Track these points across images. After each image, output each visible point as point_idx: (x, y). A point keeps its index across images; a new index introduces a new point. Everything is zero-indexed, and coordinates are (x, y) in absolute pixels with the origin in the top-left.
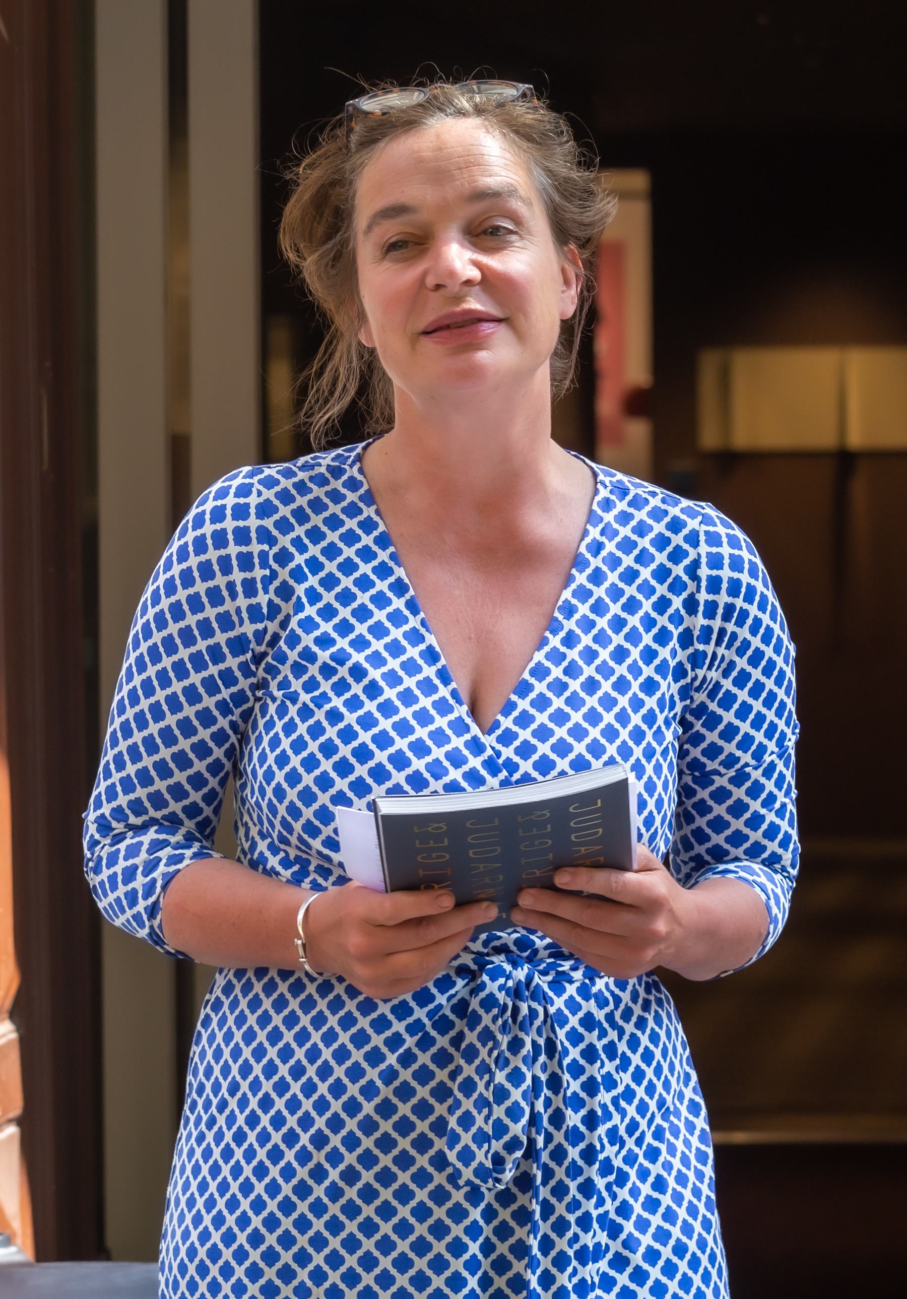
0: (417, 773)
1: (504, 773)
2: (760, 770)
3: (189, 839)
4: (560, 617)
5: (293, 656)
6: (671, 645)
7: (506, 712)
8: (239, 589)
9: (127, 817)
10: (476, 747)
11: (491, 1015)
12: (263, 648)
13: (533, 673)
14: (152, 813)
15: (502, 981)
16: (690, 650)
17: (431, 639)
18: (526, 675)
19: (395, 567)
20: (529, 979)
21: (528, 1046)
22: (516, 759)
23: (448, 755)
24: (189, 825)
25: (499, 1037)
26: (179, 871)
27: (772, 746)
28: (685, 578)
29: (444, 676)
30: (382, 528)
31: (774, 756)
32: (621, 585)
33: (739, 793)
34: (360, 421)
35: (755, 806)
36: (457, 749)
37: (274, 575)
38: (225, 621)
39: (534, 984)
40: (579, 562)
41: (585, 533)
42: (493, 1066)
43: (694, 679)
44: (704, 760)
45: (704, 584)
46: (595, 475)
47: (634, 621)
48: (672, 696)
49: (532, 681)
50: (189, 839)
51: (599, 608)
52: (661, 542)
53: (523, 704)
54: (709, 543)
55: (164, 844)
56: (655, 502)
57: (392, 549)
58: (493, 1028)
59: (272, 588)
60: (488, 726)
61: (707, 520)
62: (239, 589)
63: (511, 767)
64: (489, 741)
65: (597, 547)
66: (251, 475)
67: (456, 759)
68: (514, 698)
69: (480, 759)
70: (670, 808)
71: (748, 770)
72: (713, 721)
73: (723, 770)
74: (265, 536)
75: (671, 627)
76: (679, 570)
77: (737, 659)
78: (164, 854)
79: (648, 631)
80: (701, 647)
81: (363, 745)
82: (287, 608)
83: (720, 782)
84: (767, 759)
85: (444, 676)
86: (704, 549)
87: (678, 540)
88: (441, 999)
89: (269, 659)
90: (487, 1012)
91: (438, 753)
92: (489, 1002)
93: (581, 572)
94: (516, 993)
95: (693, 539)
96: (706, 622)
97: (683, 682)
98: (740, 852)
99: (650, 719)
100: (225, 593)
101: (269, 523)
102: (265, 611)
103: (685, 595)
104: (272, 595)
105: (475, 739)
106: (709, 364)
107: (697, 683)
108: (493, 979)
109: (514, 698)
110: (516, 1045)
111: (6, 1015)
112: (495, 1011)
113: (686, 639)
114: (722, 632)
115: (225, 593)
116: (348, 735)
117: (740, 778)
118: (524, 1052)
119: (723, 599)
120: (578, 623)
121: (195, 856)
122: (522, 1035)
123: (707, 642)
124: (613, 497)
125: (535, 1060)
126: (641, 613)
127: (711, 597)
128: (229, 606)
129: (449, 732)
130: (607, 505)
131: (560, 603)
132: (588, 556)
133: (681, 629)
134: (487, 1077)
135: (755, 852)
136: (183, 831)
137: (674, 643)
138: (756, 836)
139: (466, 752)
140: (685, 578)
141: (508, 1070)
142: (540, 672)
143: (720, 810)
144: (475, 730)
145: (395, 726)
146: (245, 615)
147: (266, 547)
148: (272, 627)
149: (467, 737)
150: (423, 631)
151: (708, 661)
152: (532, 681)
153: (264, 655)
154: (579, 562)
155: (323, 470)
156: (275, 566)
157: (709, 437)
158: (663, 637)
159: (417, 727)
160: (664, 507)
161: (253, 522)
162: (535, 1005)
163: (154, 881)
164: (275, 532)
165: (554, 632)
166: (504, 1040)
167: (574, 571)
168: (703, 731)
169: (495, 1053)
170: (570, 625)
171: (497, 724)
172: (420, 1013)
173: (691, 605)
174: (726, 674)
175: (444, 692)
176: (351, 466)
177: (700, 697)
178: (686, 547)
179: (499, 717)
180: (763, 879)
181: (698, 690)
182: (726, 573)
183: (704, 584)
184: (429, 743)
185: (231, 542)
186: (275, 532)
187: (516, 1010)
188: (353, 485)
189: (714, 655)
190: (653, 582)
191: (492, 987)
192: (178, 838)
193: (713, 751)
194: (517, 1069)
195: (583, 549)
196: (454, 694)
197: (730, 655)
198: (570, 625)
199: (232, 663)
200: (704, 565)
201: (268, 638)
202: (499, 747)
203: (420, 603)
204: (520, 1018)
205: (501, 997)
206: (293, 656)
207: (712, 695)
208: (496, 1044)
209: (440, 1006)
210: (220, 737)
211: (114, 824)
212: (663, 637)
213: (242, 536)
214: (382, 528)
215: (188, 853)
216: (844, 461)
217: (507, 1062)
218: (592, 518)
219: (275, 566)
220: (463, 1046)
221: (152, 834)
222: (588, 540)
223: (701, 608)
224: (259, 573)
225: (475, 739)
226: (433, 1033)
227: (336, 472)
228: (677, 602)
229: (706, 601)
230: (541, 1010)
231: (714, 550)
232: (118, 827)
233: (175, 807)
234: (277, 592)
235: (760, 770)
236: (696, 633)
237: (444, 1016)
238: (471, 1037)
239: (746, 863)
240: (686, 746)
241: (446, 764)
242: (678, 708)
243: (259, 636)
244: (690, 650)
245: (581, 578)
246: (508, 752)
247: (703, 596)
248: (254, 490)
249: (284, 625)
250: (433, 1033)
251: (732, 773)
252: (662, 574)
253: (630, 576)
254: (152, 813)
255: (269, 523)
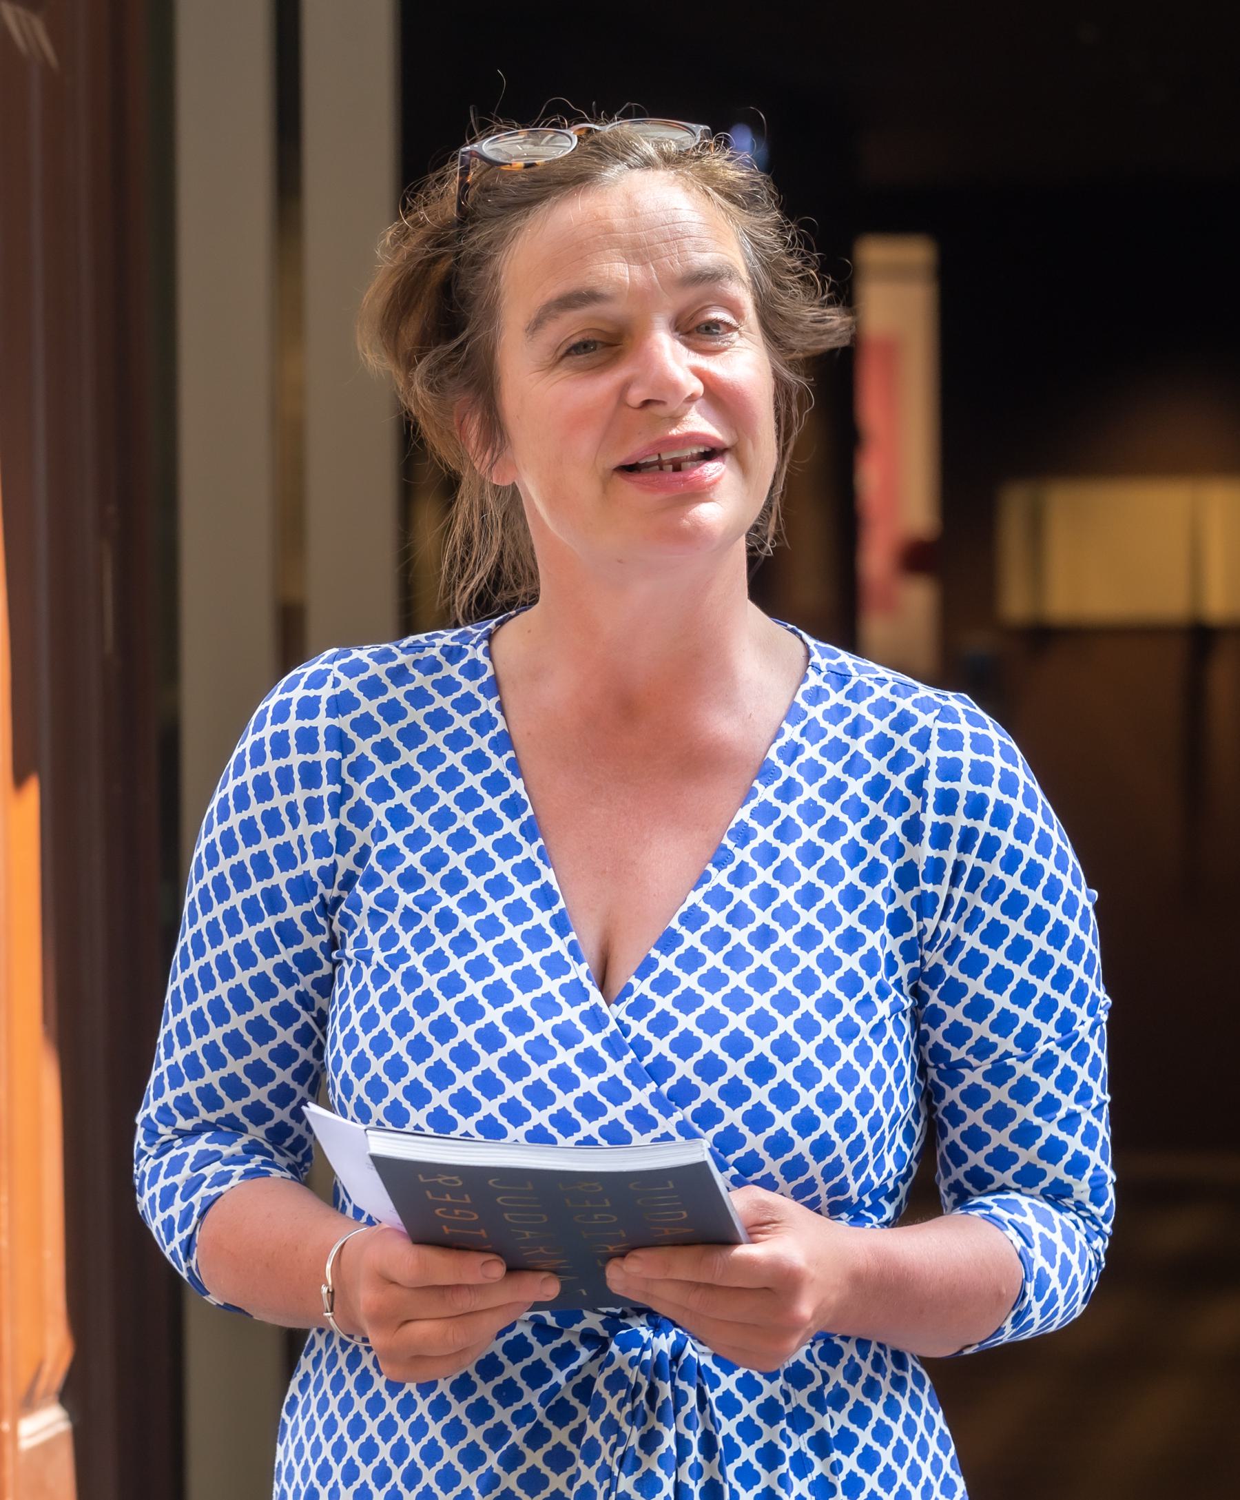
0: (513, 1055)
1: (631, 1055)
2: (1030, 1064)
3: (252, 1149)
4: (730, 845)
5: (368, 900)
6: (884, 883)
7: (642, 974)
8: (302, 812)
9: (175, 1119)
10: (595, 1020)
11: (617, 1398)
12: (335, 892)
13: (684, 920)
14: (204, 1115)
15: (636, 1352)
16: (915, 892)
17: (548, 875)
18: (675, 924)
19: (512, 779)
20: (678, 1350)
21: (669, 1440)
22: (649, 1036)
23: (556, 1031)
24: (257, 1133)
25: (626, 1429)
26: (221, 1194)
27: (1048, 1029)
28: (907, 793)
29: (561, 924)
30: (502, 725)
31: (1052, 1045)
32: (822, 802)
33: (999, 1094)
34: (505, 593)
35: (1026, 1113)
36: (569, 1023)
37: (347, 791)
38: (286, 857)
39: (684, 1356)
40: (767, 773)
41: (779, 733)
42: (616, 1470)
43: (922, 932)
44: (947, 1046)
45: (931, 800)
46: (809, 655)
47: (833, 850)
48: (890, 956)
49: (682, 931)
50: (252, 1149)
51: (786, 832)
52: (881, 745)
53: (667, 963)
54: (943, 745)
55: (216, 1156)
56: (881, 692)
57: (510, 754)
58: (620, 1417)
59: (344, 810)
60: (616, 992)
61: (947, 714)
62: (302, 812)
63: (641, 1047)
64: (616, 1012)
65: (791, 752)
66: (332, 660)
67: (567, 1036)
68: (655, 953)
69: (600, 1036)
70: (334, 1026)
71: (1009, 1061)
72: (954, 992)
73: (974, 1062)
74: (339, 741)
75: (884, 860)
76: (898, 782)
77: (985, 906)
78: (209, 1171)
79: (853, 865)
80: (929, 888)
81: (491, 1026)
82: (362, 837)
83: (973, 1077)
84: (1041, 1047)
85: (561, 924)
86: (935, 752)
87: (903, 741)
88: (559, 1377)
89: (343, 907)
90: (613, 1394)
91: (543, 1027)
92: (617, 1381)
93: (767, 785)
94: (657, 1369)
95: (922, 741)
96: (935, 853)
97: (907, 936)
98: (1006, 1177)
99: (851, 984)
100: (285, 818)
101: (344, 722)
102: (333, 840)
103: (906, 816)
104: (344, 819)
105: (595, 1009)
106: (1014, 504)
107: (927, 938)
108: (624, 1350)
109: (655, 953)
110: (650, 1441)
111: (53, 1397)
112: (622, 1393)
113: (907, 877)
114: (959, 867)
115: (285, 818)
116: (470, 1011)
117: (999, 1073)
118: (661, 1449)
119: (960, 821)
120: (754, 853)
121: (247, 1174)
122: (659, 1426)
123: (937, 880)
124: (826, 686)
125: (680, 1460)
126: (844, 840)
127: (942, 819)
128: (290, 835)
129: (560, 999)
130: (816, 696)
131: (732, 825)
132: (779, 763)
133: (900, 862)
134: (606, 1484)
135: (1029, 1177)
136: (244, 1140)
137: (889, 880)
138: (1027, 1156)
139: (581, 1027)
140: (907, 793)
141: (638, 1475)
142: (693, 919)
143: (975, 1117)
144: (596, 996)
145: (535, 1003)
146: (309, 847)
147: (336, 755)
148: (345, 863)
149: (585, 1006)
150: (539, 863)
151: (940, 908)
152: (682, 931)
153: (338, 901)
154: (767, 773)
155: (435, 652)
156: (349, 780)
157: (1016, 604)
158: (873, 874)
159: (517, 992)
160: (892, 698)
161: (322, 722)
162: (682, 1385)
163: (191, 1207)
164: (352, 735)
165: (720, 865)
166: (634, 1436)
167: (756, 784)
168: (942, 1005)
169: (620, 1451)
170: (743, 855)
171: (629, 989)
172: (532, 1397)
173: (913, 830)
174: (970, 927)
175: (559, 945)
176: (475, 646)
177: (934, 957)
178: (912, 750)
179: (634, 981)
180: (1030, 1220)
181: (929, 946)
182: (964, 786)
183: (931, 800)
184: (532, 1013)
185: (294, 749)
186: (352, 735)
187: (653, 1393)
188: (473, 670)
189: (949, 898)
190: (865, 799)
191: (620, 1358)
192: (236, 1148)
193: (958, 1034)
194: (650, 1473)
195: (772, 755)
196: (573, 948)
197: (976, 900)
198: (743, 855)
199: (293, 912)
200: (932, 775)
201: (339, 877)
202: (628, 1020)
203: (544, 822)
204: (659, 1404)
205: (633, 1374)
206: (368, 900)
207: (950, 955)
208: (622, 1439)
209: (557, 1387)
210: (285, 1014)
211: (161, 1129)
212: (873, 874)
213: (307, 740)
214: (502, 725)
215: (239, 1169)
216: (1200, 639)
217: (637, 1463)
218: (794, 714)
219: (349, 780)
220: (530, 1426)
221: (201, 1144)
222: (781, 742)
223: (927, 834)
224: (326, 789)
225: (595, 1009)
226: (548, 1424)
227: (453, 654)
228: (894, 825)
229: (935, 825)
230: (692, 1393)
231: (818, 1064)
232: (165, 1132)
233: (233, 1107)
234: (352, 815)
235: (1030, 1064)
236: (922, 868)
237: (563, 1401)
238: (593, 1430)
239: (1013, 1196)
240: (924, 1027)
241: (554, 1042)
242: (903, 970)
243: (328, 874)
244: (915, 892)
245: (766, 793)
246: (639, 1028)
247: (930, 818)
248: (330, 679)
249: (361, 859)
250: (548, 1424)
251: (987, 1065)
252: (877, 788)
253: (835, 790)
254: (204, 1115)
255: (344, 722)
